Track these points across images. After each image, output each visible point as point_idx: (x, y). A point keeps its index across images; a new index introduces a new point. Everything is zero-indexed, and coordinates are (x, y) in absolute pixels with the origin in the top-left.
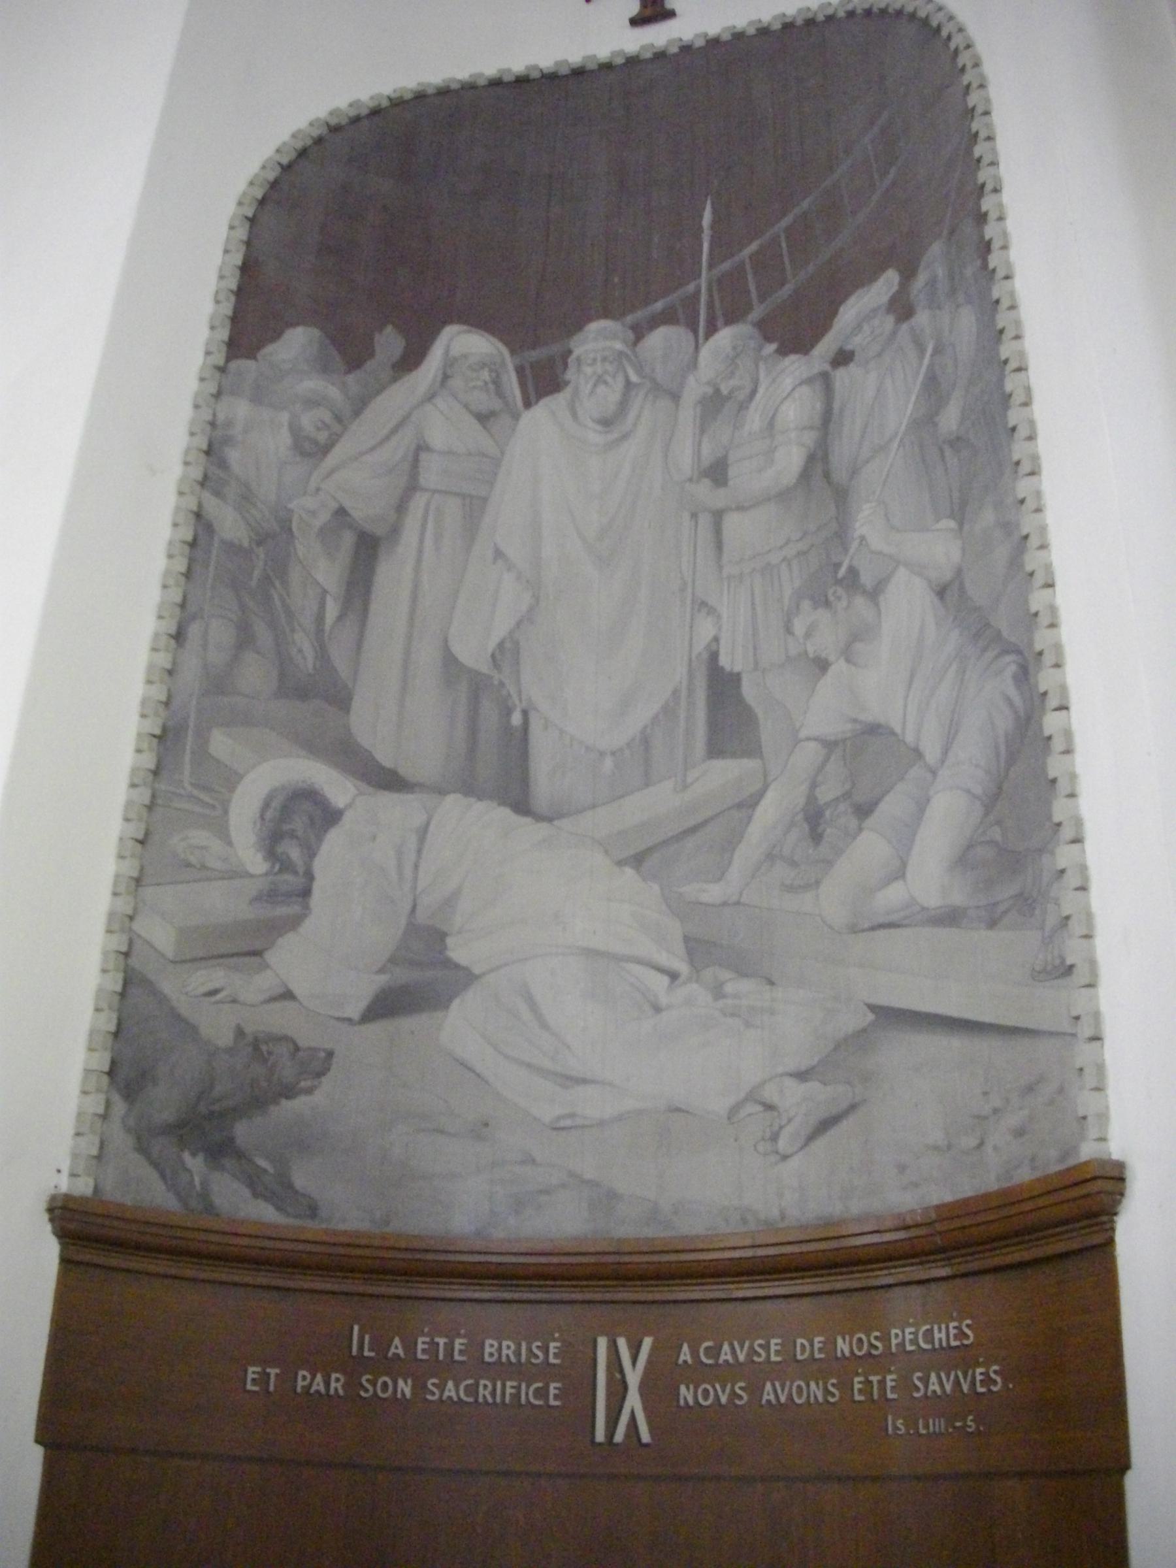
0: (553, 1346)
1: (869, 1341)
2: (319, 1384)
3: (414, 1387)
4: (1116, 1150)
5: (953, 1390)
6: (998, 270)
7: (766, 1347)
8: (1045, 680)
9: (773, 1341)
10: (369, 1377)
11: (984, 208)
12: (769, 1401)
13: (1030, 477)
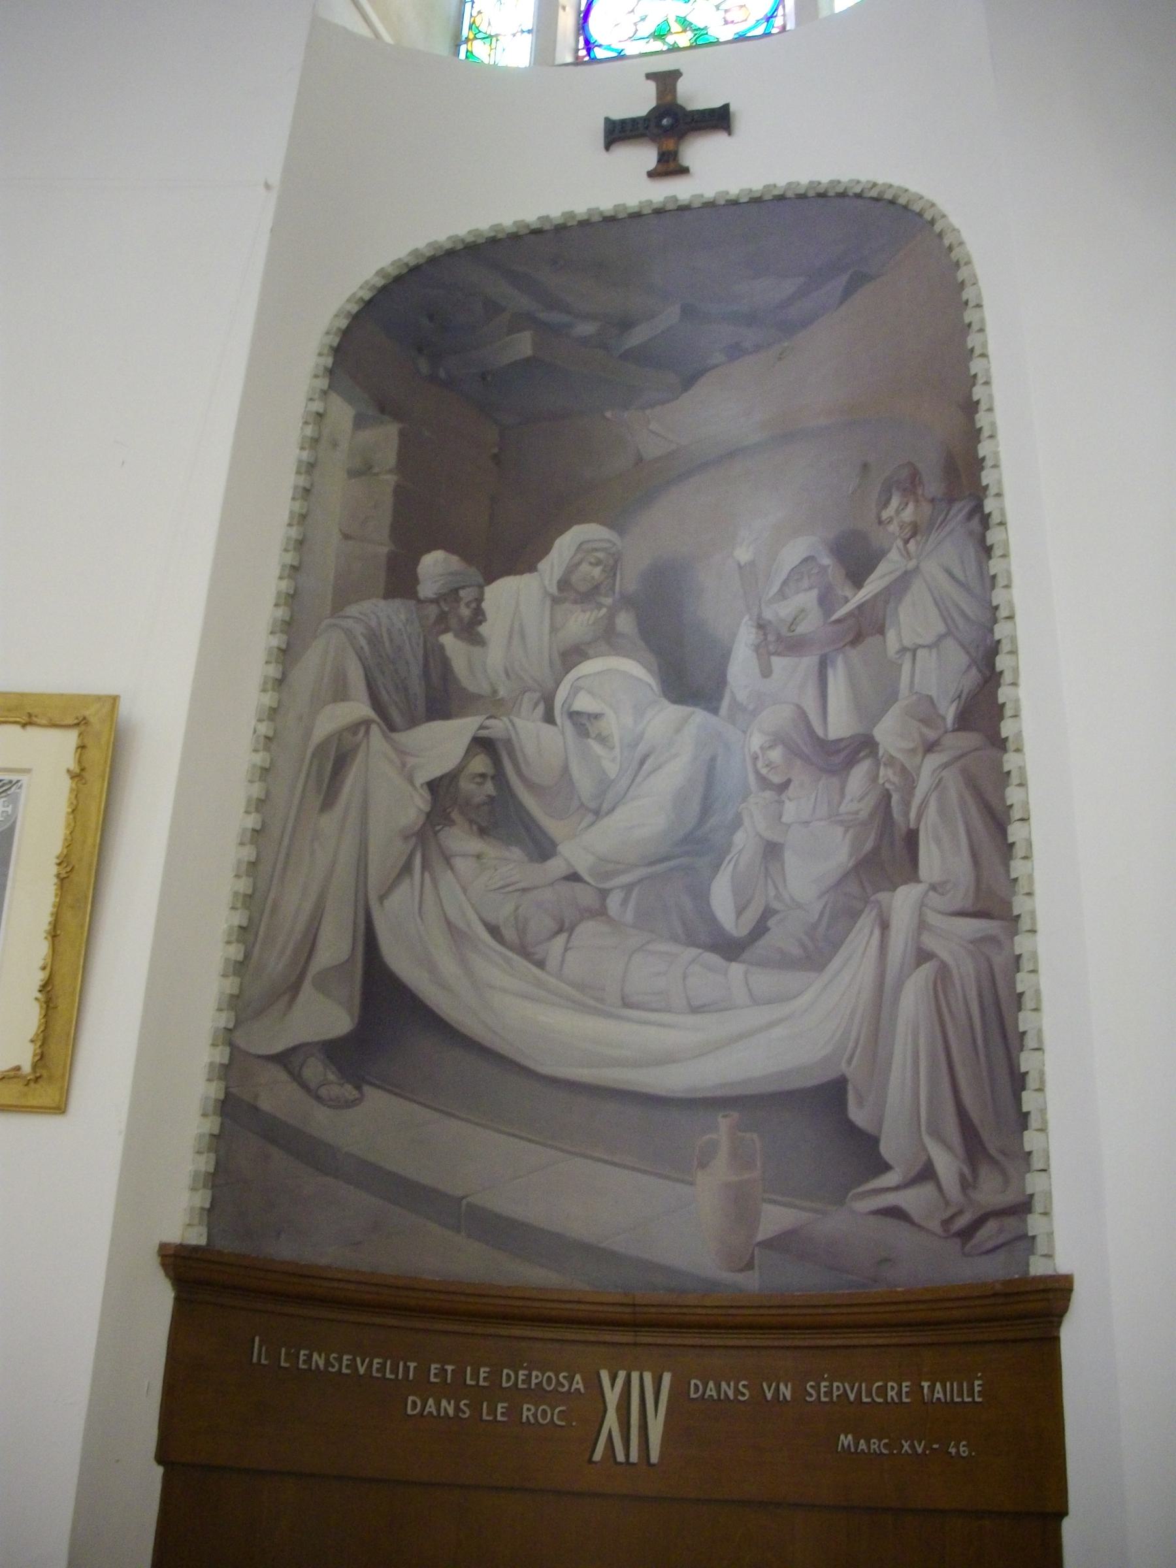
0: (500, 1408)
1: (558, 1380)
2: (711, 1390)
3: (793, 1392)
4: (1063, 1264)
5: (856, 1398)
6: (990, 487)
7: (340, 1360)
8: (982, 419)
9: (345, 1357)
10: (812, 1383)
11: (981, 454)
12: (430, 1413)
13: (1011, 687)
